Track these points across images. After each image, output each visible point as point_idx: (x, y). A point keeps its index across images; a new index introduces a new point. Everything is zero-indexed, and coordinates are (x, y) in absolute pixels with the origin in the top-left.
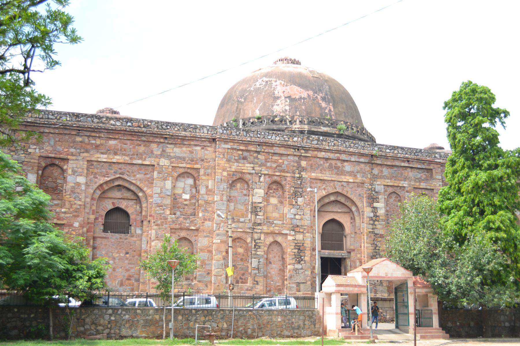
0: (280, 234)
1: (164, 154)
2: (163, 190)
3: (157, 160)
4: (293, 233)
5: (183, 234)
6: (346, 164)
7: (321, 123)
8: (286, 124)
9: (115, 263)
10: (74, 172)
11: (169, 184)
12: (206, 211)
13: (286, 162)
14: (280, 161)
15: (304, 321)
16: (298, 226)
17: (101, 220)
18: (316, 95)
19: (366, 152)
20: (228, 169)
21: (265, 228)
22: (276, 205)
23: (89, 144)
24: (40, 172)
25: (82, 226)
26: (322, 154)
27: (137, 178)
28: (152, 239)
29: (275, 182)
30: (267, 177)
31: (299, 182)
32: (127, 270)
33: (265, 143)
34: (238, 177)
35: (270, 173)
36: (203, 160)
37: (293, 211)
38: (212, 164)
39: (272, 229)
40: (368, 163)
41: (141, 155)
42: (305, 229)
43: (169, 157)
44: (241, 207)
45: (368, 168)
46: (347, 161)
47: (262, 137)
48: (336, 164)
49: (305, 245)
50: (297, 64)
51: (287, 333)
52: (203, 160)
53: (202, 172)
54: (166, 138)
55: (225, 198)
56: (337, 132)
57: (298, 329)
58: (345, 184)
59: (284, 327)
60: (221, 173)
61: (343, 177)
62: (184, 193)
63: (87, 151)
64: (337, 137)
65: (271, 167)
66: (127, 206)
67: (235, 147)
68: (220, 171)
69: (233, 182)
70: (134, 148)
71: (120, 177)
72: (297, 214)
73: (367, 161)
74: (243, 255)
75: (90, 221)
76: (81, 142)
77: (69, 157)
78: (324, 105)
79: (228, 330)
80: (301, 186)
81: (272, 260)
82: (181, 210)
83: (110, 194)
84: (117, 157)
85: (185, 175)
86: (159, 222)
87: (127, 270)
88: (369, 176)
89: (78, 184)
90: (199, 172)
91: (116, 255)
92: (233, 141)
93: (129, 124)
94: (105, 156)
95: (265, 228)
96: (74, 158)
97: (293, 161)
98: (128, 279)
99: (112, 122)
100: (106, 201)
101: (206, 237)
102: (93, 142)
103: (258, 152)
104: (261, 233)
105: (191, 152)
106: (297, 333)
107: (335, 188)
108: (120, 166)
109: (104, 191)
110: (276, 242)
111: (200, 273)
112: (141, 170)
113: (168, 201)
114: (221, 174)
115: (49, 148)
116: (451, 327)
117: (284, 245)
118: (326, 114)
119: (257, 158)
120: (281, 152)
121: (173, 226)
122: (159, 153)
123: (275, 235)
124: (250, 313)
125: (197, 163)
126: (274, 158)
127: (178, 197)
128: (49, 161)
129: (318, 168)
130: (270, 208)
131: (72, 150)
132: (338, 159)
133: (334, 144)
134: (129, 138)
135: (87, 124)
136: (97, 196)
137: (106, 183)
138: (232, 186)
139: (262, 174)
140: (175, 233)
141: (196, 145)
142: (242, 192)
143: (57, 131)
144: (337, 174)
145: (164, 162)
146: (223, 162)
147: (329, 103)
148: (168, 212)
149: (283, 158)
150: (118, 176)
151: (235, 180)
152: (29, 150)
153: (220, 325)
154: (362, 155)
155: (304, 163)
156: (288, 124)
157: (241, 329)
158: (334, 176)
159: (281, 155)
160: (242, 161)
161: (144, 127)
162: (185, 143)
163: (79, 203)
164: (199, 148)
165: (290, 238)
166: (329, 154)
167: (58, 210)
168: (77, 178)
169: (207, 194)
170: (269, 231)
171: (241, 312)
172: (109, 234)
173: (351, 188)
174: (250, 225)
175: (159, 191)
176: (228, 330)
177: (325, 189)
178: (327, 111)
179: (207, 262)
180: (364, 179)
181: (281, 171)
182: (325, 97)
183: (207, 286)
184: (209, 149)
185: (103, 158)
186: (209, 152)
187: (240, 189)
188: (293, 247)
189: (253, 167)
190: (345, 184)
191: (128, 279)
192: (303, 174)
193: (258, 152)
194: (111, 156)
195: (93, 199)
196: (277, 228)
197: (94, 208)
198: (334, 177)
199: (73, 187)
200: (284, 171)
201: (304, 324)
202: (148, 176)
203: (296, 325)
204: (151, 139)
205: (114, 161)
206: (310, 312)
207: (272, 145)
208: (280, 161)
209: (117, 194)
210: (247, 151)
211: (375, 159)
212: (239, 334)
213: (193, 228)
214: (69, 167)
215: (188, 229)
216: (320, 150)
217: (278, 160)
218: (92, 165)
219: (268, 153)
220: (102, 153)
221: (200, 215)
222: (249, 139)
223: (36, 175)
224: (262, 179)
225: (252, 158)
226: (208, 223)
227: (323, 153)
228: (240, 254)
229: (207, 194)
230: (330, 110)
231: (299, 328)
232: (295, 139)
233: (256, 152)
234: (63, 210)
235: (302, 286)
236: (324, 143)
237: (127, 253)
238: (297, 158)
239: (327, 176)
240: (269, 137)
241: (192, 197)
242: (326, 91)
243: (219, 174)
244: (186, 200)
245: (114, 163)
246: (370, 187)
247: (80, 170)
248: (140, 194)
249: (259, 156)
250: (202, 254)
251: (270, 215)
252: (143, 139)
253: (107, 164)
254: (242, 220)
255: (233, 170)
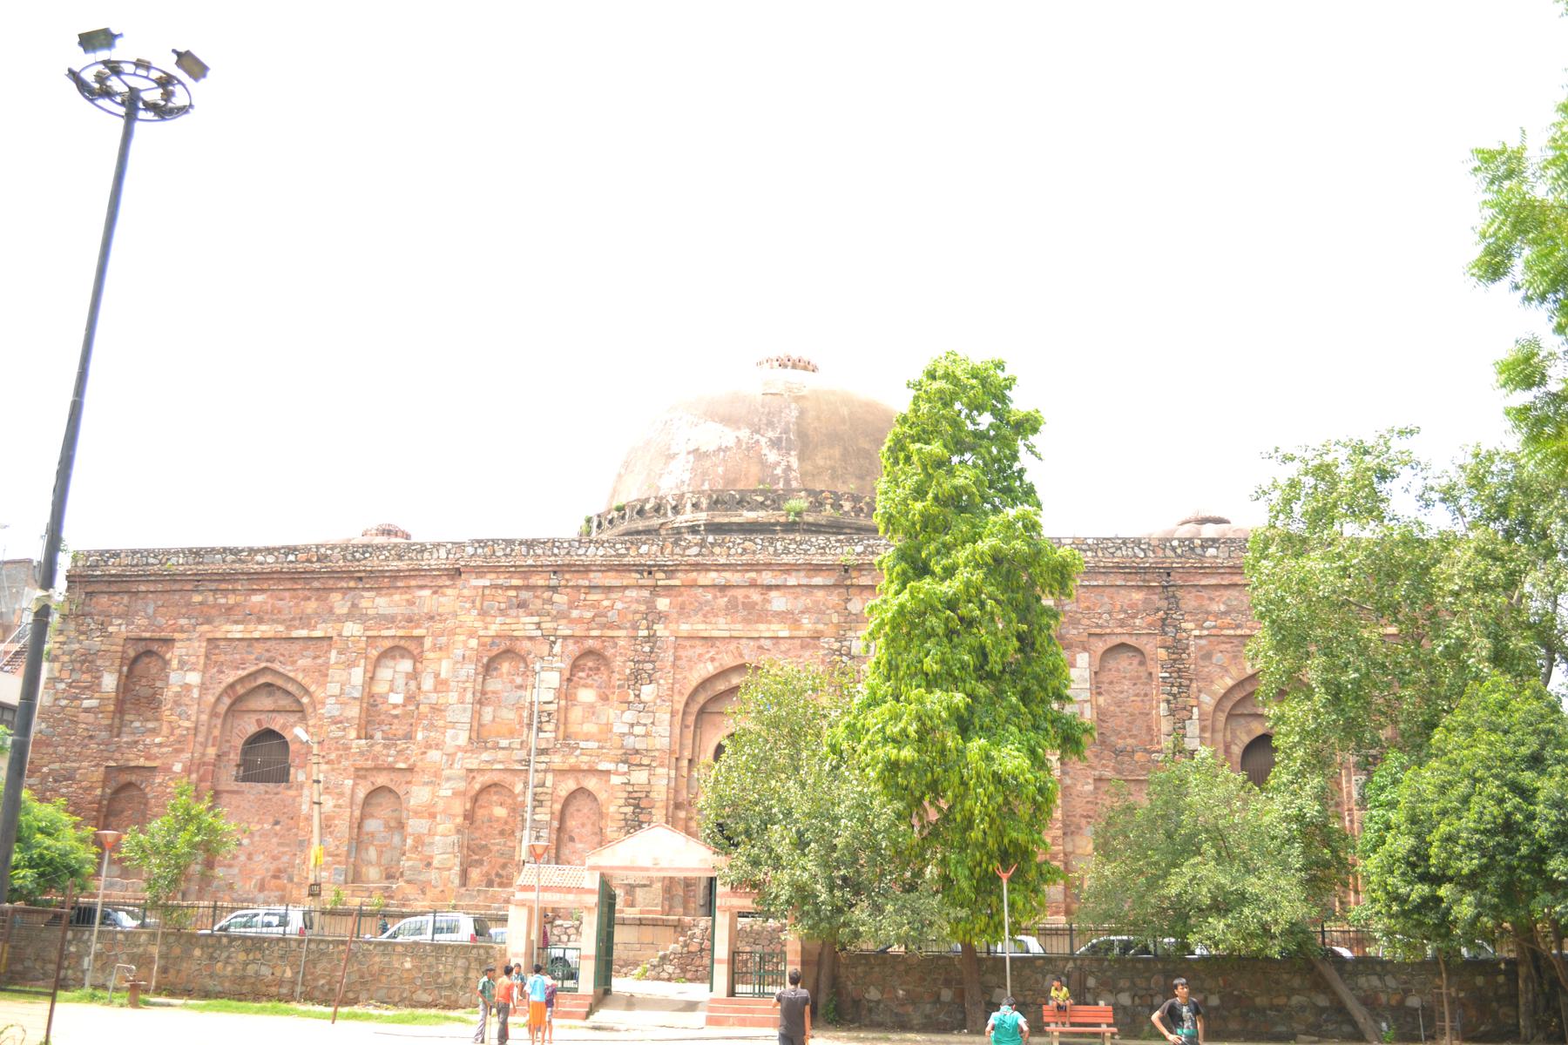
0: (593, 771)
1: (354, 614)
2: (347, 689)
3: (338, 626)
4: (623, 768)
5: (381, 780)
6: (773, 594)
7: (741, 503)
8: (665, 514)
9: (252, 843)
10: (182, 664)
11: (357, 675)
12: (432, 726)
13: (619, 605)
14: (606, 603)
15: (467, 970)
16: (637, 752)
17: (235, 757)
18: (757, 437)
19: (829, 559)
20: (481, 633)
21: (557, 760)
22: (592, 706)
23: (214, 606)
24: (125, 669)
25: (188, 770)
26: (712, 577)
27: (298, 668)
28: (321, 791)
29: (590, 653)
30: (570, 642)
31: (647, 649)
32: (275, 858)
33: (568, 565)
34: (503, 647)
35: (578, 633)
36: (432, 618)
37: (629, 716)
38: (450, 623)
39: (572, 760)
40: (835, 586)
41: (309, 617)
42: (654, 758)
43: (363, 618)
44: (508, 715)
45: (834, 598)
46: (777, 587)
47: (563, 552)
48: (747, 597)
49: (652, 795)
50: (805, 368)
51: (426, 997)
52: (432, 618)
53: (428, 643)
54: (360, 579)
55: (469, 697)
56: (782, 520)
57: (450, 988)
58: (767, 644)
59: (419, 982)
60: (465, 643)
61: (762, 627)
62: (392, 690)
63: (208, 621)
64: (783, 531)
65: (580, 620)
66: (284, 727)
67: (500, 582)
68: (462, 638)
69: (492, 660)
70: (297, 605)
71: (266, 668)
72: (638, 723)
73: (830, 581)
74: (506, 823)
75: (206, 759)
76: (201, 603)
77: (176, 636)
78: (772, 456)
79: (294, 983)
80: (651, 657)
81: (576, 833)
82: (385, 728)
83: (254, 703)
84: (263, 627)
85: (397, 654)
86: (333, 756)
87: (275, 858)
88: (835, 618)
89: (187, 687)
90: (422, 644)
91: (255, 827)
92: (495, 569)
93: (291, 558)
94: (240, 627)
95: (557, 760)
96: (185, 636)
97: (638, 601)
98: (275, 877)
99: (259, 558)
100: (246, 717)
101: (427, 784)
102: (222, 601)
103: (554, 589)
104: (546, 771)
105: (411, 603)
106: (447, 997)
107: (741, 655)
108: (269, 643)
109: (237, 700)
110: (581, 791)
111: (410, 863)
112: (306, 649)
113: (354, 712)
114: (465, 645)
115: (145, 622)
116: (878, 1002)
117: (602, 796)
118: (775, 479)
119: (550, 601)
120: (607, 582)
121: (361, 763)
122: (345, 611)
123: (580, 775)
124: (342, 947)
125: (418, 626)
126: (590, 597)
127: (380, 700)
128: (141, 647)
129: (696, 613)
130: (576, 714)
131: (183, 621)
132: (753, 585)
133: (744, 549)
134: (289, 585)
135: (210, 568)
136: (222, 708)
137: (241, 680)
138: (489, 668)
139: (557, 637)
140: (365, 777)
141: (421, 587)
142: (512, 681)
143: (160, 587)
144: (746, 621)
145: (352, 629)
146: (471, 619)
147: (788, 450)
148: (353, 734)
149: (613, 596)
150: (263, 665)
151: (497, 656)
152: (110, 629)
153: (278, 973)
154: (817, 569)
155: (663, 604)
156: (670, 513)
157: (322, 982)
158: (739, 626)
159: (609, 589)
160: (513, 612)
161: (319, 560)
162: (399, 584)
163: (187, 724)
164: (427, 592)
165: (616, 780)
166: (727, 575)
167: (148, 741)
168: (186, 678)
169: (435, 690)
170: (566, 767)
171: (322, 946)
172: (245, 786)
173: (785, 653)
174: (522, 754)
175: (337, 691)
176: (294, 983)
177: (712, 659)
178: (779, 471)
179: (427, 840)
180: (821, 627)
181: (603, 626)
182: (779, 439)
183: (424, 893)
184: (449, 591)
185: (237, 631)
186: (447, 600)
187: (509, 673)
188: (622, 802)
189: (538, 624)
190: (767, 644)
191: (275, 877)
192: (660, 629)
193: (554, 589)
194: (251, 627)
195: (214, 714)
196: (585, 759)
197: (216, 732)
198: (739, 629)
199: (178, 694)
200: (611, 626)
201: (467, 979)
202: (320, 661)
203: (447, 978)
204: (331, 583)
205: (257, 635)
206: (482, 951)
207: (586, 569)
208: (606, 603)
209: (266, 702)
210: (528, 588)
211: (854, 574)
212: (317, 994)
213: (402, 766)
214: (174, 655)
215: (392, 769)
216: (705, 568)
217: (599, 601)
218: (217, 647)
219: (578, 587)
220: (236, 622)
221: (420, 736)
222: (530, 562)
223: (116, 676)
224: (557, 649)
225: (539, 602)
226: (434, 755)
227: (713, 575)
228: (498, 819)
229: (435, 690)
230: (789, 468)
231: (453, 985)
232: (644, 549)
233: (549, 587)
234: (158, 740)
235: (639, 892)
236: (717, 550)
237: (277, 823)
238: (646, 593)
239: (721, 627)
240: (581, 551)
241: (410, 699)
242: (788, 423)
243: (460, 645)
244: (395, 706)
245: (257, 639)
246: (836, 646)
247: (193, 659)
248: (305, 700)
249: (556, 597)
250: (417, 821)
251: (573, 728)
252: (316, 584)
253: (245, 643)
254: (504, 743)
255: (492, 633)
